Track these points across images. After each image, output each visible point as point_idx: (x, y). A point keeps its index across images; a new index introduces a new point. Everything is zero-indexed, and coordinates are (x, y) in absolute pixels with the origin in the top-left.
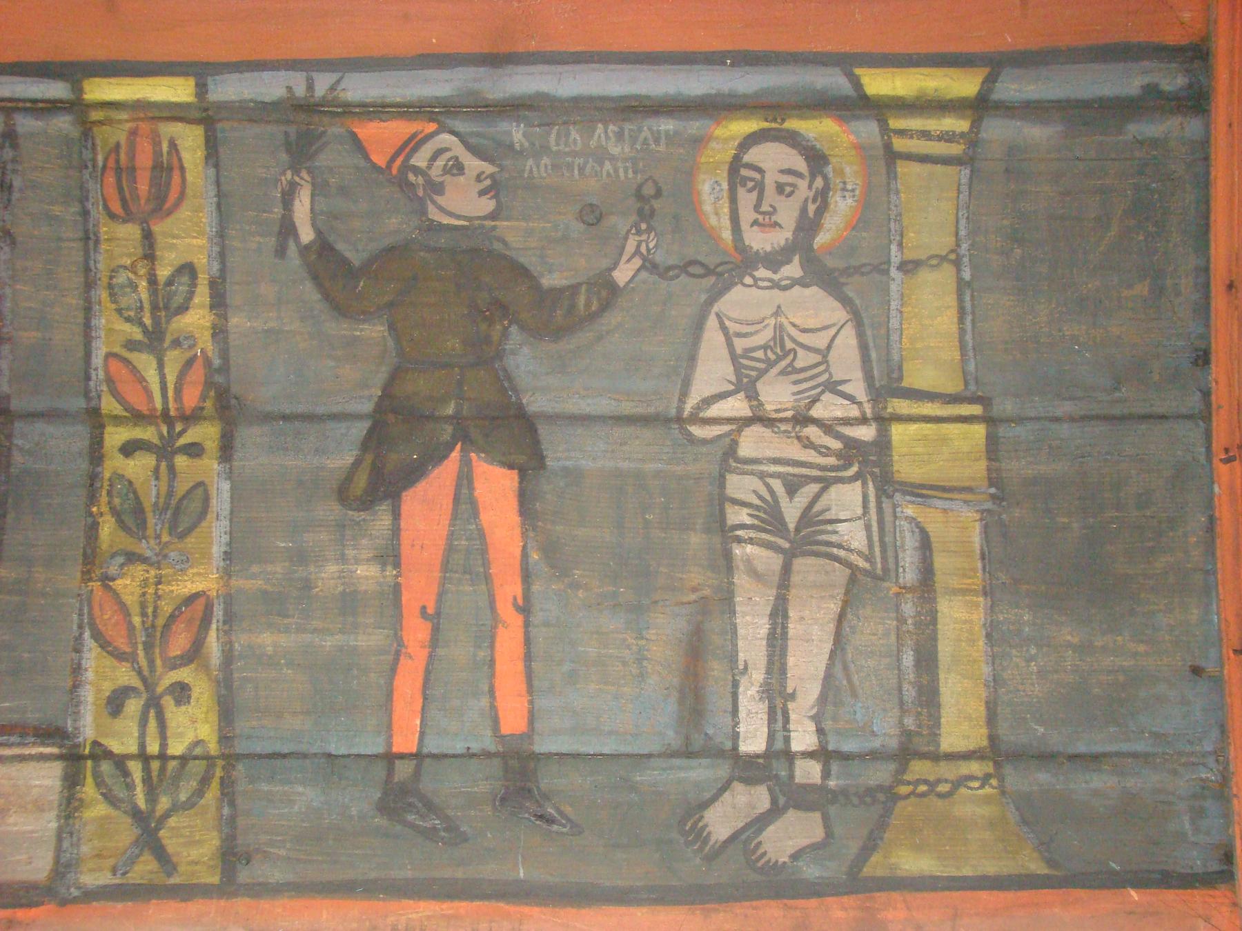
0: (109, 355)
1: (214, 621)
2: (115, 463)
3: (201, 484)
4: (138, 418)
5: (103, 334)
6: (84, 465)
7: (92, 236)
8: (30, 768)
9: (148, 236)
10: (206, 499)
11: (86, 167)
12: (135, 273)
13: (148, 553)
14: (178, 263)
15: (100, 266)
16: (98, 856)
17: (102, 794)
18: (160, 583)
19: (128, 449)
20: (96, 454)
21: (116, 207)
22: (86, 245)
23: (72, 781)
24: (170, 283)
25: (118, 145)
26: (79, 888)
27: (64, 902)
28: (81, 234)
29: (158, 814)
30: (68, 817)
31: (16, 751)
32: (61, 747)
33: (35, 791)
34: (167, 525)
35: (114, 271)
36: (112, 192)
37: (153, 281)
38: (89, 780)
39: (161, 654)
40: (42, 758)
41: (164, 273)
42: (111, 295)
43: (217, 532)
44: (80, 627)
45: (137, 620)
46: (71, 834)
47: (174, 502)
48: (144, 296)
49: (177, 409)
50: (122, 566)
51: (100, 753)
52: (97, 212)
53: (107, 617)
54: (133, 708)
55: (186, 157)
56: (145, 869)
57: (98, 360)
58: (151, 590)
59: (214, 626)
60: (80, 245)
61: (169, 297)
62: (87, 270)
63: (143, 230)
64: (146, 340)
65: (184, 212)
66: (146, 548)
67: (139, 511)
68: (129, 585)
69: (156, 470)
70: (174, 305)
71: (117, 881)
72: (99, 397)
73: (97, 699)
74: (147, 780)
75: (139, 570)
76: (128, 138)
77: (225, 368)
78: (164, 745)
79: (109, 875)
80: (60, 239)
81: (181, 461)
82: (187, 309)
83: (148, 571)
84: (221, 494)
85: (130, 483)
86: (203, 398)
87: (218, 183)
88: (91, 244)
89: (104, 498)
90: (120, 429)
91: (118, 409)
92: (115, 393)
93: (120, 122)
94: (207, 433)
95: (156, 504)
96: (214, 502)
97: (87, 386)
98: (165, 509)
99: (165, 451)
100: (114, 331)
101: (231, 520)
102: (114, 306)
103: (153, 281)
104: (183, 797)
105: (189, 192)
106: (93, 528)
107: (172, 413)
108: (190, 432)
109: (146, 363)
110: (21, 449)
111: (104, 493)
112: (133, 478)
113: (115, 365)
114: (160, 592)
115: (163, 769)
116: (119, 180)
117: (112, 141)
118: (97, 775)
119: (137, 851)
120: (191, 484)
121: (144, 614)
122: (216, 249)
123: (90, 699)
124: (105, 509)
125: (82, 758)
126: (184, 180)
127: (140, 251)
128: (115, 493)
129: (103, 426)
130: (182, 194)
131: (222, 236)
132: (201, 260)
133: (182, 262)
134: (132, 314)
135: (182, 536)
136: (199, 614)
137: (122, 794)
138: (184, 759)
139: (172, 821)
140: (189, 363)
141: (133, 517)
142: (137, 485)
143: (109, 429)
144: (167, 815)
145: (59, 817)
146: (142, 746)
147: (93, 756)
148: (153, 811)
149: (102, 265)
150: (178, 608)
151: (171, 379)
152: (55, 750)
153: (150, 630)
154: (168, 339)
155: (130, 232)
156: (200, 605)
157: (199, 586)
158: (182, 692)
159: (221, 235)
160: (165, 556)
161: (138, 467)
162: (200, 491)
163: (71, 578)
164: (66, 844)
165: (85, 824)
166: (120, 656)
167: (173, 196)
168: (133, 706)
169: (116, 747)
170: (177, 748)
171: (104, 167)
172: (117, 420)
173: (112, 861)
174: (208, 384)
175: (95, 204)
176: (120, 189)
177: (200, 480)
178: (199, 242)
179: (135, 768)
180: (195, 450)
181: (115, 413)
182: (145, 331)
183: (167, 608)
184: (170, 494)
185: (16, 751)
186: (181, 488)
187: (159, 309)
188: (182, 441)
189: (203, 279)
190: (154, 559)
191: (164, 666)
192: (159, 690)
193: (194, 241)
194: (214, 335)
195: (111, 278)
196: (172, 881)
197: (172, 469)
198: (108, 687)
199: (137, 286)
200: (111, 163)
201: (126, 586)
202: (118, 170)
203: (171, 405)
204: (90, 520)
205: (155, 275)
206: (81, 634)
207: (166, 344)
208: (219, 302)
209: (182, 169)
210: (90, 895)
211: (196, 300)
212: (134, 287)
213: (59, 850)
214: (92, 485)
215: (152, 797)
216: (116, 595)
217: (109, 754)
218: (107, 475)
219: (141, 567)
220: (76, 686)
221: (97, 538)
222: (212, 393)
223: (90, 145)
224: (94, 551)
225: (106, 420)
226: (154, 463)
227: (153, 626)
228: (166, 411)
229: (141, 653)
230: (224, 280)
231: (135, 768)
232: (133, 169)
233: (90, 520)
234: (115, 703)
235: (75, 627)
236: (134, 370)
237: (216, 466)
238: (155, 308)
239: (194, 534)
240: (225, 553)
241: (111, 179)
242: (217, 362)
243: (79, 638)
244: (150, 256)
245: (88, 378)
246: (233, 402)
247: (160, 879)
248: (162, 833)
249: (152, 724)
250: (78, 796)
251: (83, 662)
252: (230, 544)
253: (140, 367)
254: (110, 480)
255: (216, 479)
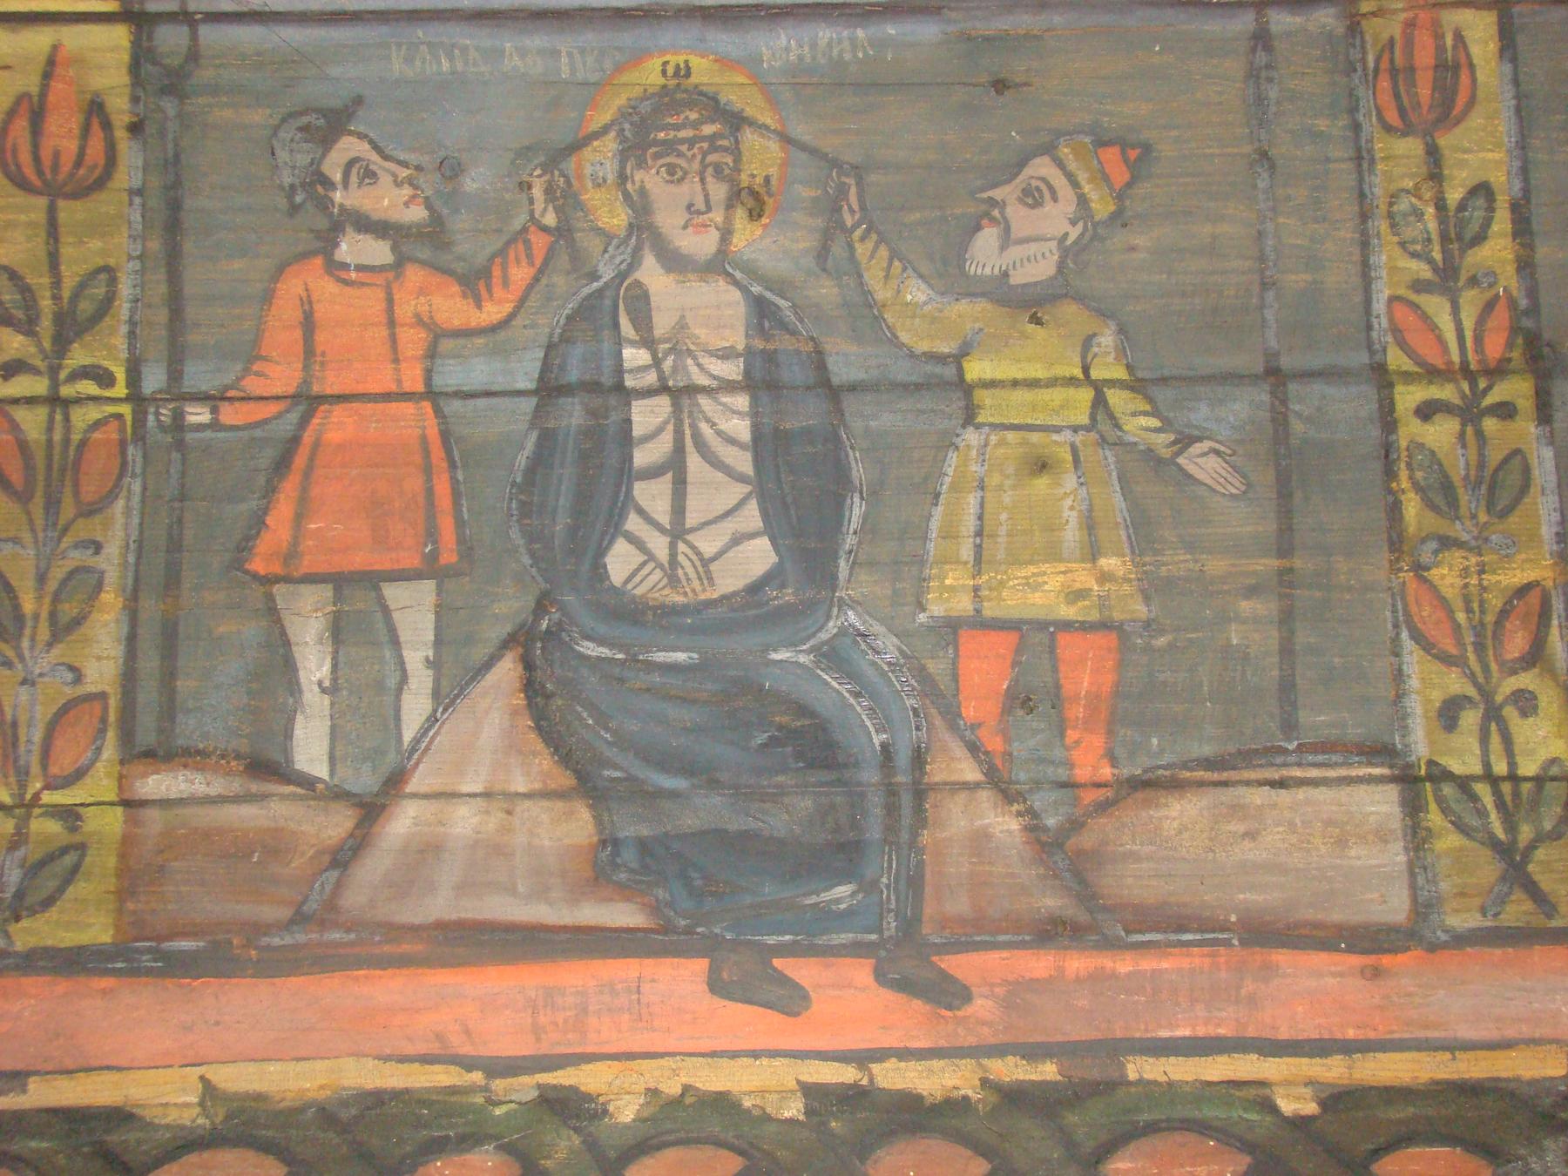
0: (1393, 299)
1: (1555, 616)
2: (1411, 429)
3: (1517, 452)
4: (1432, 374)
5: (1384, 273)
6: (1375, 432)
7: (1365, 154)
8: (1361, 791)
9: (1433, 152)
10: (1526, 470)
11: (1355, 70)
12: (1420, 198)
13: (1465, 537)
14: (1471, 183)
15: (1376, 190)
16: (1462, 894)
17: (1452, 823)
18: (1481, 572)
19: (1426, 412)
20: (1388, 419)
21: (1392, 117)
22: (1360, 165)
23: (1413, 807)
24: (1462, 206)
25: (1392, 41)
26: (1446, 931)
27: (1433, 948)
28: (1352, 153)
29: (1522, 845)
30: (1417, 849)
31: (1343, 772)
32: (1391, 767)
33: (1372, 819)
34: (1483, 503)
35: (1393, 197)
36: (1386, 98)
37: (1440, 205)
38: (1433, 806)
39: (1495, 655)
40: (1370, 780)
41: (1454, 196)
42: (1393, 226)
43: (1544, 510)
44: (1396, 626)
45: (1461, 617)
46: (1425, 869)
47: (1488, 473)
48: (1432, 225)
49: (1479, 362)
50: (1436, 552)
51: (1439, 775)
52: (1370, 125)
53: (1426, 613)
54: (1471, 720)
55: (1476, 51)
56: (1518, 911)
57: (1379, 306)
58: (1474, 581)
59: (1555, 622)
60: (1350, 166)
61: (1462, 224)
62: (1362, 195)
63: (1427, 144)
64: (1437, 279)
65: (1476, 120)
66: (1459, 531)
67: (1447, 487)
68: (1447, 575)
69: (1462, 435)
70: (1468, 235)
71: (1489, 924)
72: (1384, 350)
73: (1426, 711)
74: (1500, 805)
75: (1456, 557)
76: (1404, 32)
77: (1534, 310)
78: (1512, 765)
79: (1478, 916)
80: (1328, 160)
81: (1490, 424)
82: (1485, 238)
83: (1465, 558)
84: (1544, 463)
85: (1433, 453)
86: (1510, 345)
87: (1516, 82)
88: (1365, 166)
89: (1404, 474)
90: (1412, 388)
91: (1408, 365)
92: (1402, 344)
93: (1395, 12)
94: (1517, 389)
95: (1466, 478)
96: (1536, 472)
97: (1369, 338)
98: (1479, 483)
99: (1469, 413)
100: (1396, 268)
101: (1560, 496)
102: (1396, 239)
103: (1440, 205)
104: (1548, 826)
105: (1480, 94)
106: (1394, 510)
107: (1473, 367)
108: (1496, 389)
109: (1437, 307)
110: (1299, 415)
111: (1403, 466)
112: (1434, 446)
113: (1400, 311)
114: (1485, 583)
115: (1516, 794)
116: (1395, 85)
117: (1385, 36)
118: (1440, 800)
119: (1505, 889)
120: (1506, 452)
121: (1469, 610)
122: (1517, 164)
123: (1419, 711)
124: (1405, 484)
125: (1417, 780)
126: (1474, 80)
127: (1424, 170)
128: (1415, 466)
129: (1391, 385)
130: (1472, 101)
131: (1523, 148)
132: (1498, 179)
133: (1475, 182)
134: (1418, 247)
135: (1504, 514)
136: (1536, 608)
137: (1475, 822)
138: (1539, 780)
139: (1540, 854)
140: (1489, 306)
141: (1441, 495)
142: (1440, 455)
143: (1399, 389)
144: (1532, 847)
145: (1406, 848)
146: (1487, 765)
147: (1430, 778)
148: (1514, 841)
149: (1378, 190)
150: (1509, 602)
151: (1468, 324)
152: (1385, 771)
153: (1479, 629)
154: (1464, 277)
155: (1410, 147)
156: (1534, 598)
157: (1530, 575)
158: (1526, 703)
159: (1522, 145)
160: (1486, 540)
161: (1440, 434)
162: (1516, 461)
163: (1376, 567)
164: (1420, 880)
165: (1438, 857)
166: (1446, 660)
167: (1461, 100)
168: (1470, 719)
169: (1457, 768)
170: (1528, 768)
171: (1376, 70)
172: (1408, 377)
173: (1477, 901)
174: (1515, 330)
175: (1368, 115)
176: (1397, 96)
177: (1514, 447)
178: (1496, 156)
179: (1483, 790)
180: (1506, 411)
181: (1404, 368)
182: (1435, 270)
183: (1495, 602)
184: (1481, 465)
185: (1343, 772)
186: (1495, 456)
187: (1451, 241)
188: (1489, 400)
189: (1502, 202)
190: (1473, 543)
191: (1501, 671)
192: (1499, 699)
193: (1490, 155)
194: (1519, 270)
195: (1391, 204)
196: (1554, 923)
197: (1480, 434)
198: (1437, 696)
199: (1422, 214)
200: (1384, 65)
201: (1443, 577)
202: (1394, 72)
203: (1471, 356)
204: (1391, 499)
205: (1444, 199)
206: (1398, 634)
207: (1461, 284)
208: (1522, 228)
209: (1471, 66)
210: (1461, 940)
211: (1495, 227)
212: (1419, 215)
213: (1413, 887)
214: (1387, 456)
215: (1511, 827)
216: (1433, 588)
217: (1448, 776)
218: (1403, 444)
219: (1458, 554)
220: (1399, 696)
221: (1401, 518)
222: (1520, 341)
223: (1358, 42)
224: (1400, 535)
225: (1394, 378)
226: (1458, 427)
227: (1482, 624)
228: (1465, 365)
229: (1471, 656)
230: (1528, 201)
231: (1483, 790)
232: (1412, 69)
233: (1391, 499)
234: (1448, 715)
235: (1390, 626)
236: (1425, 317)
237: (1533, 430)
238: (1445, 238)
239: (1517, 512)
240: (1557, 534)
241: (1385, 83)
242: (1523, 303)
243: (1396, 640)
244: (1435, 174)
245: (1369, 327)
246: (1546, 350)
247: (1539, 921)
248: (1530, 868)
249: (1495, 740)
250: (1424, 824)
251: (1405, 667)
252: (1562, 523)
253: (1430, 311)
254: (1408, 449)
255: (1535, 446)
